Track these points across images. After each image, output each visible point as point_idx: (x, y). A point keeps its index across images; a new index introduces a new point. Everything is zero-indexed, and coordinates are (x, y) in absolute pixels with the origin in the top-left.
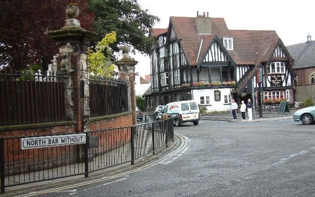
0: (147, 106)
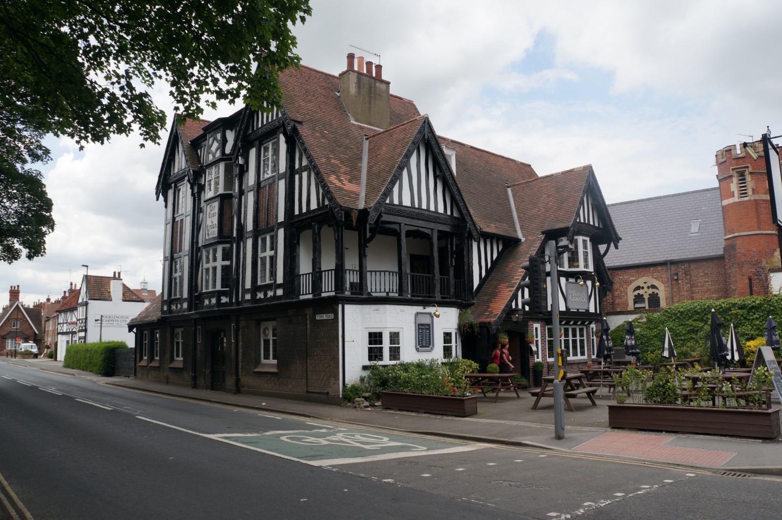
0: (141, 359)
